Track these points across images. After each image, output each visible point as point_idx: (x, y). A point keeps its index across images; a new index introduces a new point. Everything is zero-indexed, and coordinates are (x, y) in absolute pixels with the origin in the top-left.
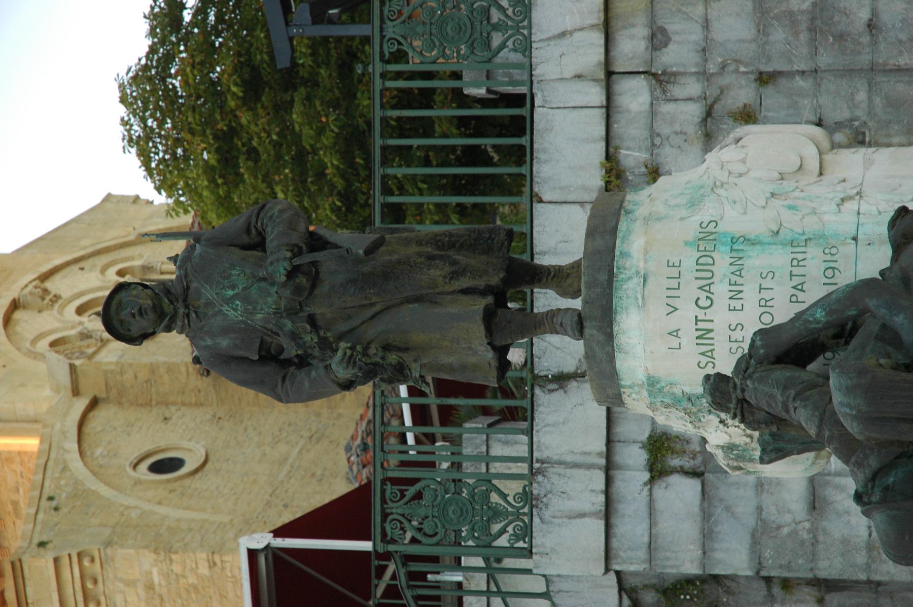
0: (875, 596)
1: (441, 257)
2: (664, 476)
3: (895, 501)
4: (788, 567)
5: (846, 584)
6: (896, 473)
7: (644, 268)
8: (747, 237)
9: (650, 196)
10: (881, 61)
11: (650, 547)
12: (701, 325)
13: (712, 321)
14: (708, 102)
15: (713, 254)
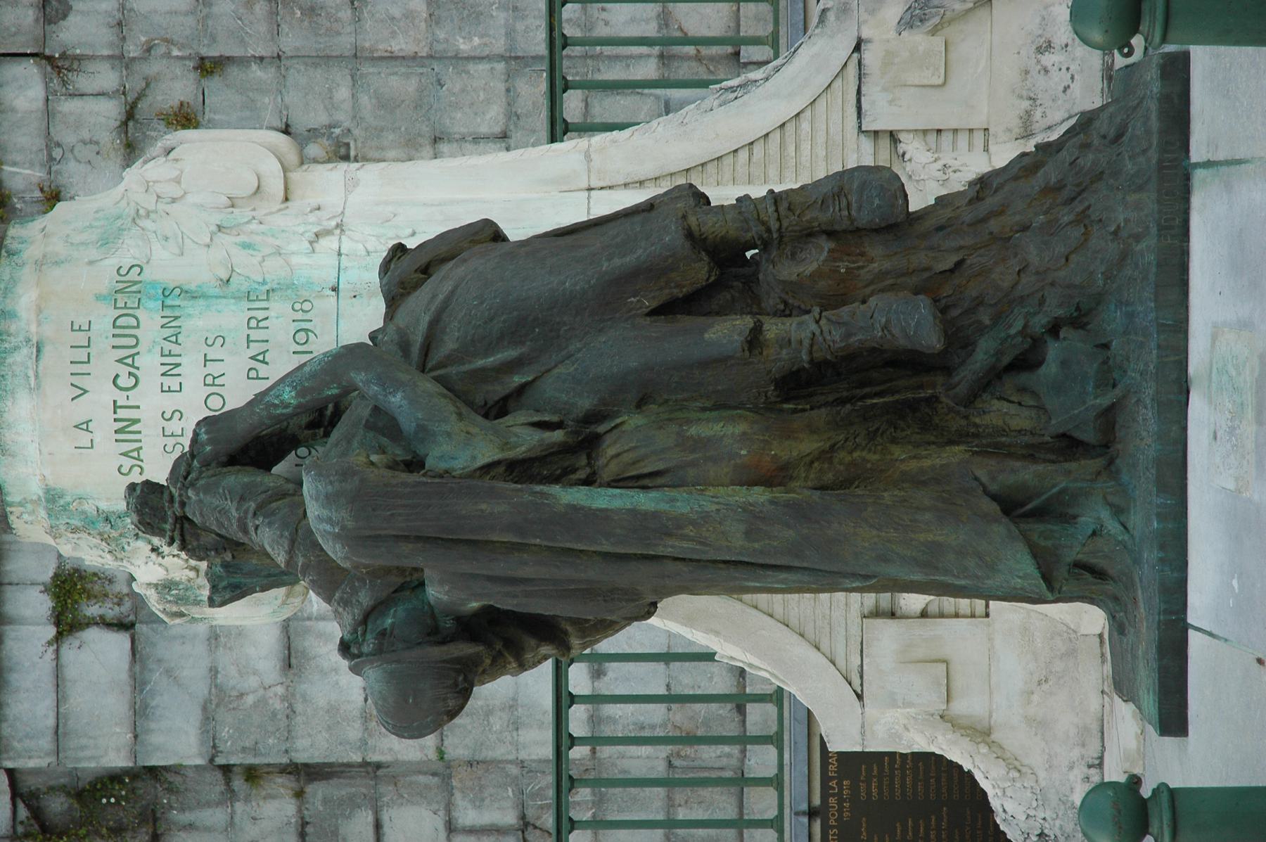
0: (372, 783)
2: (77, 631)
3: (393, 651)
4: (255, 750)
5: (334, 769)
6: (395, 611)
7: (37, 333)
8: (185, 288)
9: (43, 230)
10: (367, 45)
11: (56, 732)
12: (122, 413)
13: (138, 407)
14: (129, 98)
15: (137, 313)
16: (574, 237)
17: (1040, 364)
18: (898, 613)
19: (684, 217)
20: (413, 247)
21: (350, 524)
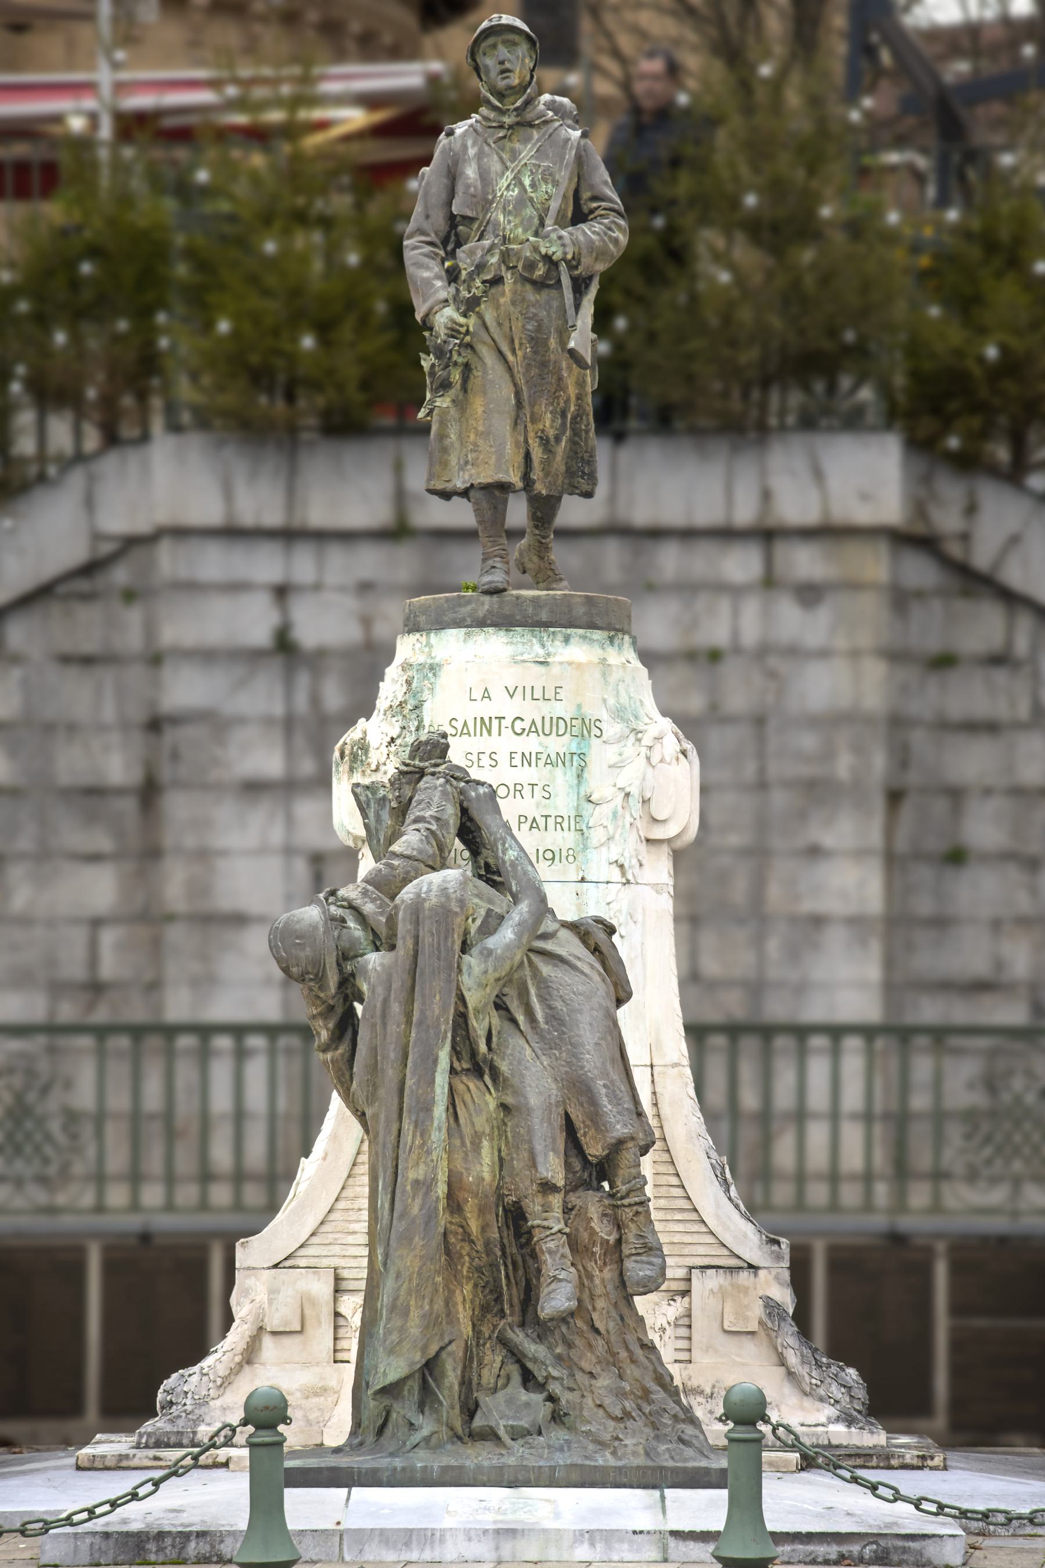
1: (564, 424)
8: (586, 770)
9: (628, 662)
12: (495, 722)
13: (500, 735)
15: (568, 735)
16: (619, 1058)
17: (527, 1389)
18: (338, 1295)
19: (633, 1138)
20: (613, 940)
21: (427, 905)
